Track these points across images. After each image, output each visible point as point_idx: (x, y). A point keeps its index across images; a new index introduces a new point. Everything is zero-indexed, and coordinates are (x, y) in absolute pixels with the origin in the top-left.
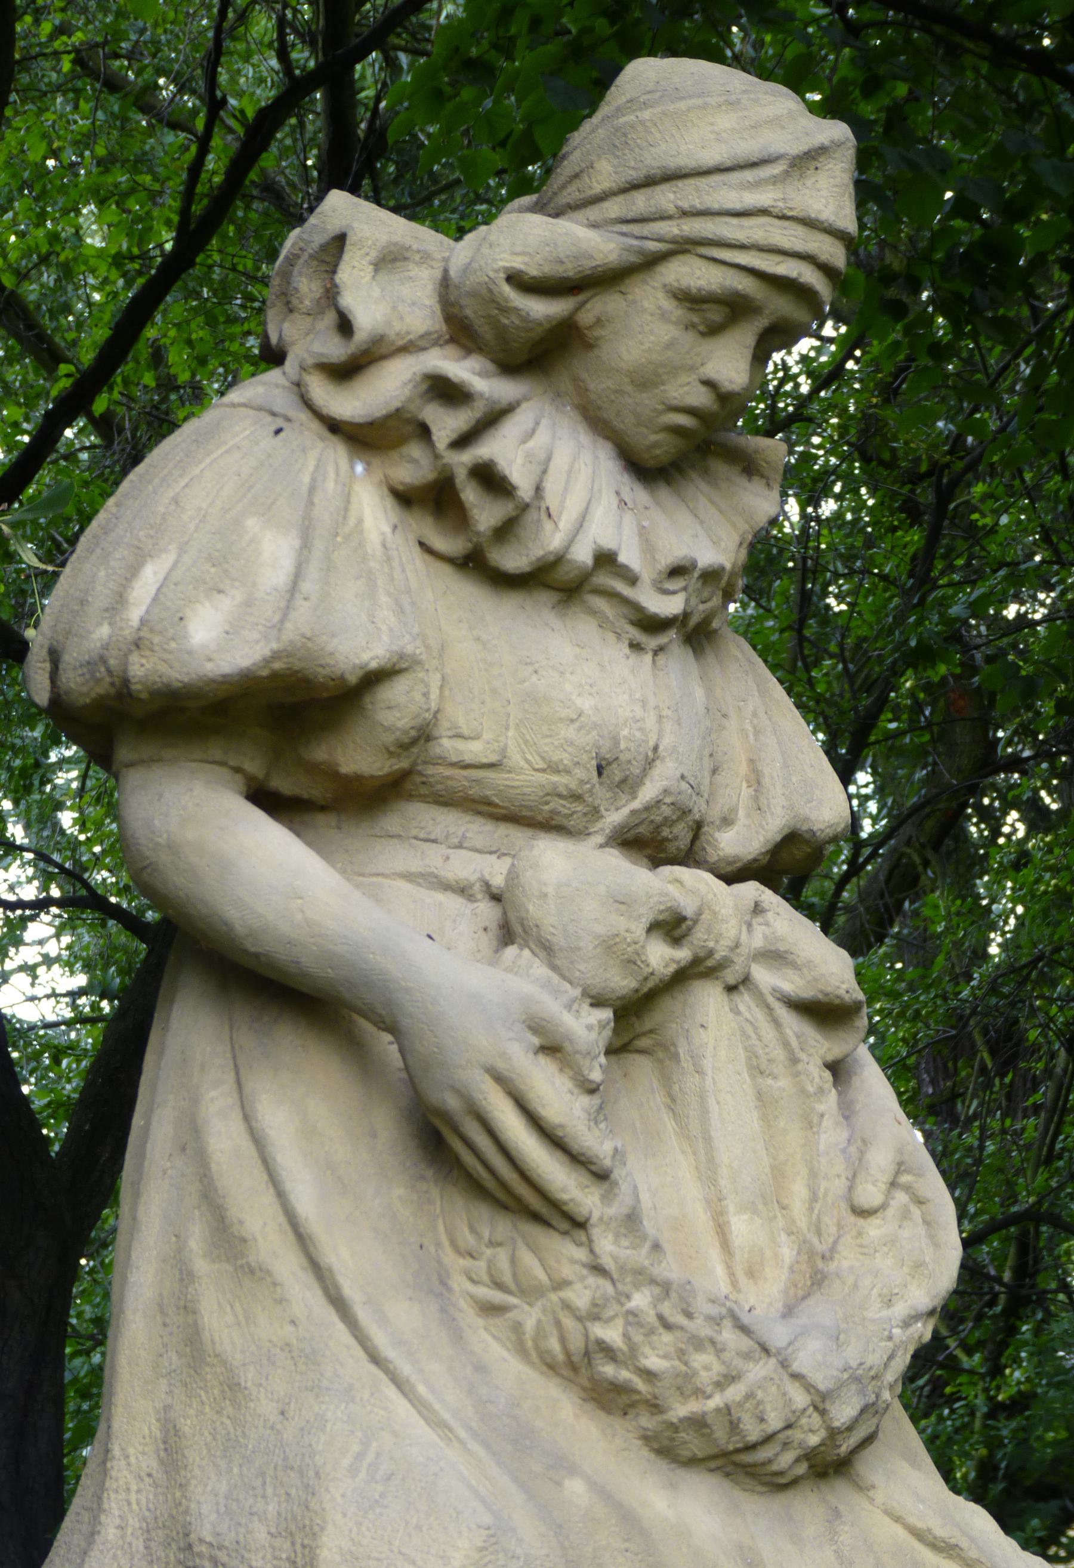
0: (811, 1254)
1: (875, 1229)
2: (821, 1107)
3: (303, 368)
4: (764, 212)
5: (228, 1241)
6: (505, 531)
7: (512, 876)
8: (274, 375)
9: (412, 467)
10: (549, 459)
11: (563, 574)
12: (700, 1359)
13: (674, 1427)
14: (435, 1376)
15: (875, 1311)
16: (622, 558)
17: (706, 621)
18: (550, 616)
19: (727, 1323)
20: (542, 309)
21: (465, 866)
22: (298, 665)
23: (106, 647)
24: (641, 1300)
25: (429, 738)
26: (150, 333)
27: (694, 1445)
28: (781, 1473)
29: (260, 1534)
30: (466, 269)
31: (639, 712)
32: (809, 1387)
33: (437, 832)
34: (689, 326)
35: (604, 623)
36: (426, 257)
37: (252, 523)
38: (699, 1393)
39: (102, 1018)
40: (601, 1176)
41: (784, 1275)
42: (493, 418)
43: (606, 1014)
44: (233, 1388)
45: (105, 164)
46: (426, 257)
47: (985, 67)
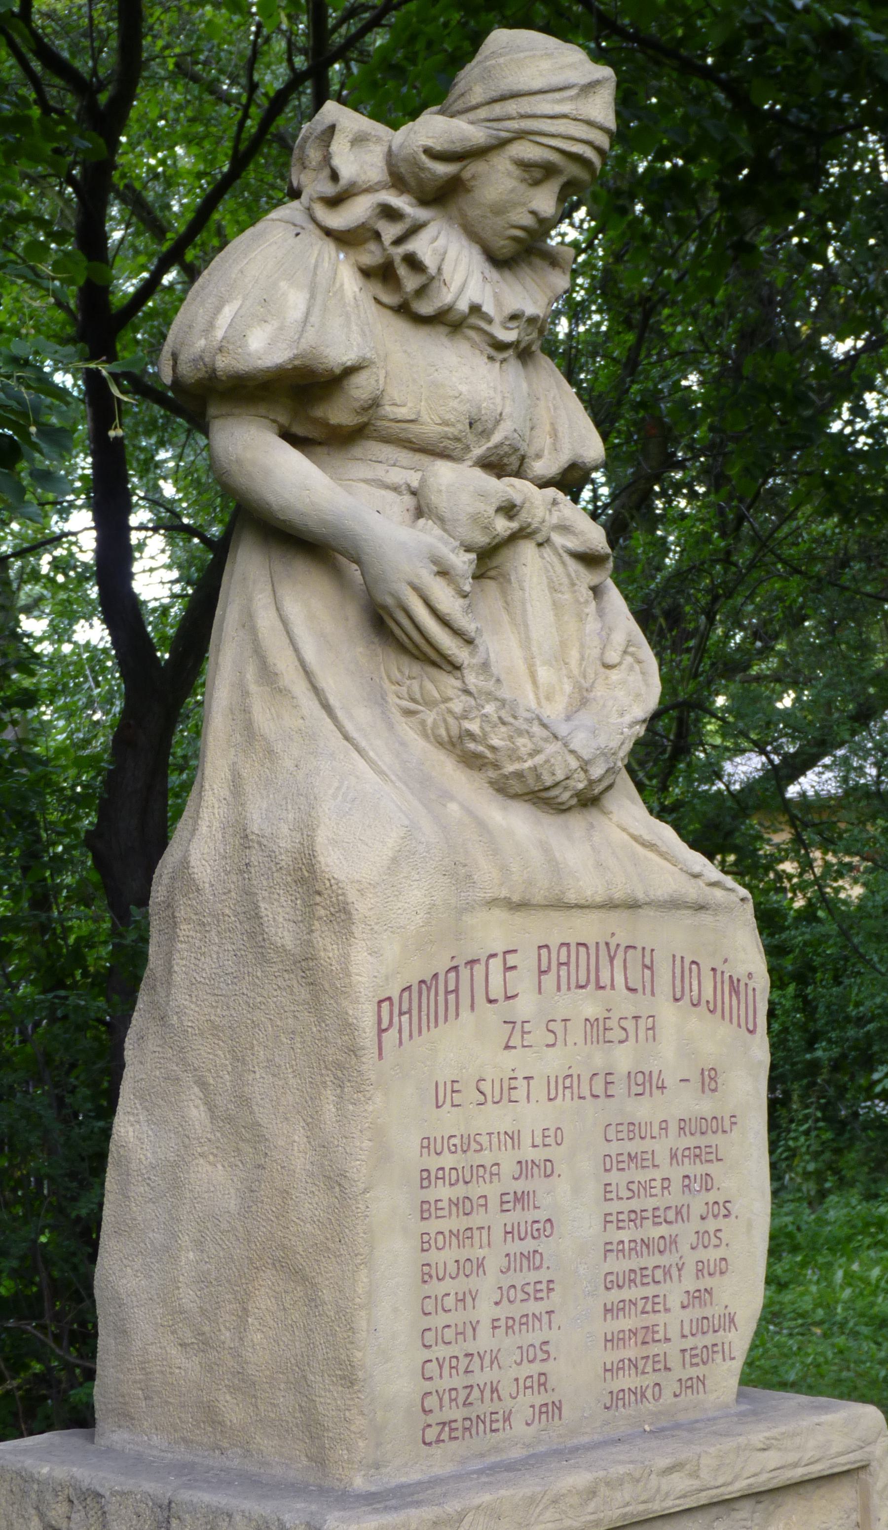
0: (580, 688)
1: (615, 676)
2: (587, 610)
3: (311, 200)
4: (565, 116)
5: (268, 674)
6: (421, 292)
7: (423, 481)
8: (295, 204)
9: (371, 256)
10: (445, 253)
11: (452, 317)
12: (521, 741)
13: (506, 777)
14: (378, 746)
15: (614, 719)
16: (485, 309)
17: (529, 346)
18: (445, 340)
19: (536, 722)
20: (442, 169)
21: (397, 476)
22: (308, 363)
23: (203, 351)
24: (489, 709)
25: (378, 405)
26: (216, 216)
27: (518, 788)
28: (562, 803)
29: (285, 829)
30: (401, 146)
31: (492, 394)
32: (578, 757)
33: (382, 457)
34: (523, 180)
35: (474, 345)
36: (379, 140)
37: (283, 284)
38: (520, 759)
39: (187, 595)
40: (469, 642)
41: (565, 700)
42: (415, 229)
43: (473, 556)
44: (270, 753)
45: (192, 120)
46: (379, 140)
47: (675, 75)
